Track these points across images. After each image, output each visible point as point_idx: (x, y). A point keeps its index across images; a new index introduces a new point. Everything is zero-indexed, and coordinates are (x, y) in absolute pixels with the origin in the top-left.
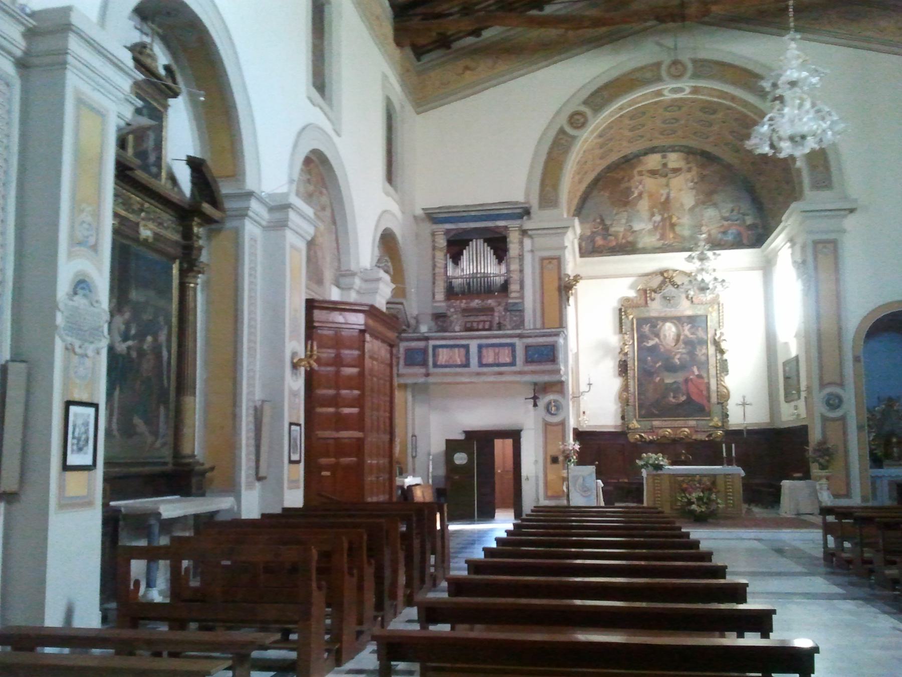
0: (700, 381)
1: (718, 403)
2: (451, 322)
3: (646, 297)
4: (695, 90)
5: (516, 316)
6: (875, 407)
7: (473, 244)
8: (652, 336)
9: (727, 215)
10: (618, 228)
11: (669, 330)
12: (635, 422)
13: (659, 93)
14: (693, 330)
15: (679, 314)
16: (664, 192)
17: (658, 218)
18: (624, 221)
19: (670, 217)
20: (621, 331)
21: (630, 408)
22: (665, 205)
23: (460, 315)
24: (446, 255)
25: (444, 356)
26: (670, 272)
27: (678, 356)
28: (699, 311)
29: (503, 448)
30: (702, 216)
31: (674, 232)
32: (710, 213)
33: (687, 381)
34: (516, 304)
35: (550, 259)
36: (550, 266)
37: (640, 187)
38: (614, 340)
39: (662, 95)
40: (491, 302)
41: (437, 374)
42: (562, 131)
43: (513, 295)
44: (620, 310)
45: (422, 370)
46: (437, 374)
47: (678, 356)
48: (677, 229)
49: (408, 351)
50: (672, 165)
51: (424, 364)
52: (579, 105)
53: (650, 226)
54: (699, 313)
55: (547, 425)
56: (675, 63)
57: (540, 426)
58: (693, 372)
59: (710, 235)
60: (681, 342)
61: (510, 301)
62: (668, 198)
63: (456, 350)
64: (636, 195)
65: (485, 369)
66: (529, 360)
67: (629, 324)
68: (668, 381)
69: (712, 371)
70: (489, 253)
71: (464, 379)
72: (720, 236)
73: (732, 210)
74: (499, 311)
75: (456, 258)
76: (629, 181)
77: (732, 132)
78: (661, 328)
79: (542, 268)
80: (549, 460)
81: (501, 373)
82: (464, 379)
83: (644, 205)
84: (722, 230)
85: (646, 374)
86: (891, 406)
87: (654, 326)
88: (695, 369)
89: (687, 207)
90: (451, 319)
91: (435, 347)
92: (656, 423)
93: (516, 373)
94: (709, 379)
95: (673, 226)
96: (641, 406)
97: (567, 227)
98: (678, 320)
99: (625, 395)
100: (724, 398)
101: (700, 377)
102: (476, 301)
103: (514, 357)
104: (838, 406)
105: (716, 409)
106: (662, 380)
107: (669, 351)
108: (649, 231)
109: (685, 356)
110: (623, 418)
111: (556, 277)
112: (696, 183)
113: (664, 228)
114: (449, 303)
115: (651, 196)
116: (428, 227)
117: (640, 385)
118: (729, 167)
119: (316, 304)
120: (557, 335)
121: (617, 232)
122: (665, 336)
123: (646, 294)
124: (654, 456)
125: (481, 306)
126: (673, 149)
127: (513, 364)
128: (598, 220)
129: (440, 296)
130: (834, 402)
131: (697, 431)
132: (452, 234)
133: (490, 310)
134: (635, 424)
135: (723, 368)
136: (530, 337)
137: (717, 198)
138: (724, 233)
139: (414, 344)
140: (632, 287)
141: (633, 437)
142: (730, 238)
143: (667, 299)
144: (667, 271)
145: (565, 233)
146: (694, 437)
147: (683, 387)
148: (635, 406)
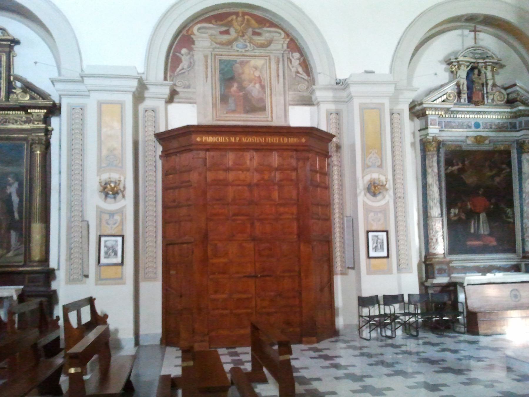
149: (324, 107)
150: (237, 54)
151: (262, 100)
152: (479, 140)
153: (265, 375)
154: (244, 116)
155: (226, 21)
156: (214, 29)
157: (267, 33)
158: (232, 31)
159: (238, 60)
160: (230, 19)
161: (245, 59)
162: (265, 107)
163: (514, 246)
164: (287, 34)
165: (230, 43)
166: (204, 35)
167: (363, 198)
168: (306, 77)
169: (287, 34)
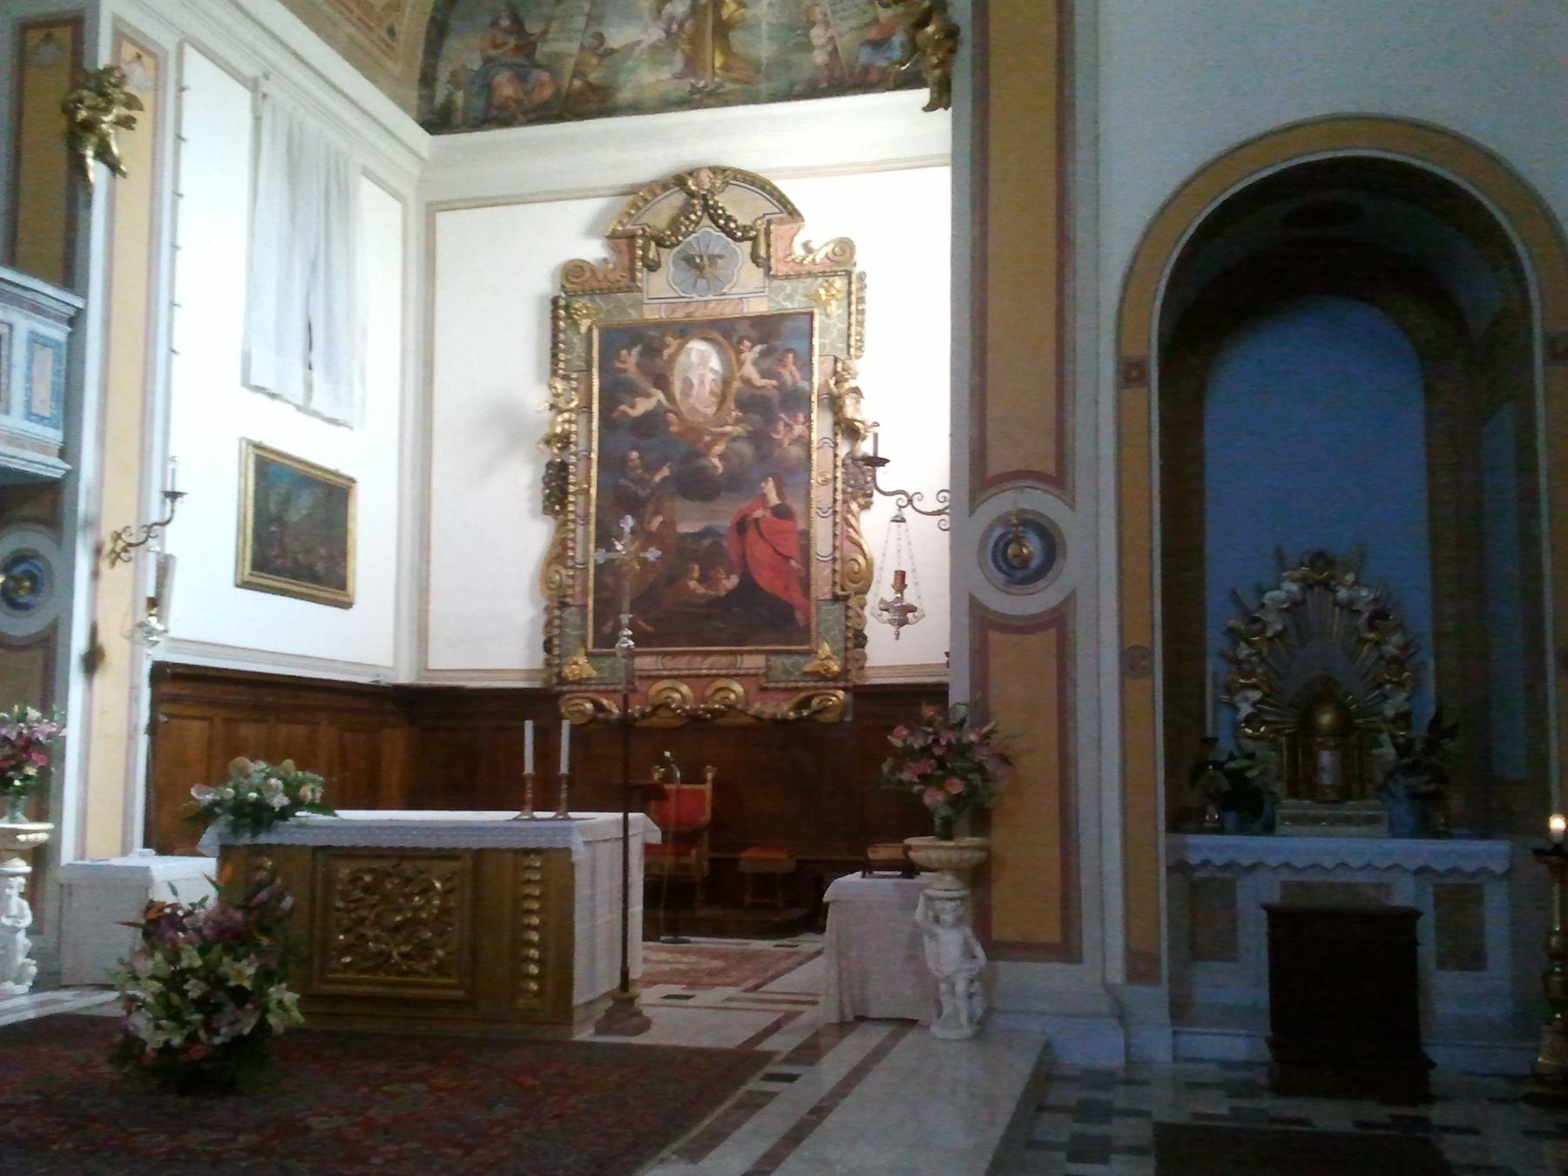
1: (836, 599)
3: (633, 259)
10: (564, 45)
11: (701, 363)
12: (582, 660)
14: (767, 363)
15: (729, 311)
18: (580, 22)
20: (554, 373)
21: (571, 615)
26: (705, 177)
27: (719, 448)
28: (790, 299)
31: (727, 51)
33: (742, 525)
35: (46, 25)
36: (48, 53)
44: (555, 301)
47: (719, 448)
48: (736, 38)
53: (656, 34)
54: (790, 306)
58: (764, 498)
69: (821, 495)
72: (865, 56)
78: (673, 358)
84: (872, 33)
87: (652, 351)
98: (724, 332)
101: (782, 512)
105: (826, 617)
107: (693, 432)
108: (655, 48)
110: (548, 646)
113: (696, 42)
121: (558, 56)
122: (688, 384)
123: (635, 244)
128: (505, 23)
131: (763, 689)
134: (580, 666)
138: (878, 45)
140: (592, 231)
143: (695, 265)
146: (757, 707)
148: (585, 606)
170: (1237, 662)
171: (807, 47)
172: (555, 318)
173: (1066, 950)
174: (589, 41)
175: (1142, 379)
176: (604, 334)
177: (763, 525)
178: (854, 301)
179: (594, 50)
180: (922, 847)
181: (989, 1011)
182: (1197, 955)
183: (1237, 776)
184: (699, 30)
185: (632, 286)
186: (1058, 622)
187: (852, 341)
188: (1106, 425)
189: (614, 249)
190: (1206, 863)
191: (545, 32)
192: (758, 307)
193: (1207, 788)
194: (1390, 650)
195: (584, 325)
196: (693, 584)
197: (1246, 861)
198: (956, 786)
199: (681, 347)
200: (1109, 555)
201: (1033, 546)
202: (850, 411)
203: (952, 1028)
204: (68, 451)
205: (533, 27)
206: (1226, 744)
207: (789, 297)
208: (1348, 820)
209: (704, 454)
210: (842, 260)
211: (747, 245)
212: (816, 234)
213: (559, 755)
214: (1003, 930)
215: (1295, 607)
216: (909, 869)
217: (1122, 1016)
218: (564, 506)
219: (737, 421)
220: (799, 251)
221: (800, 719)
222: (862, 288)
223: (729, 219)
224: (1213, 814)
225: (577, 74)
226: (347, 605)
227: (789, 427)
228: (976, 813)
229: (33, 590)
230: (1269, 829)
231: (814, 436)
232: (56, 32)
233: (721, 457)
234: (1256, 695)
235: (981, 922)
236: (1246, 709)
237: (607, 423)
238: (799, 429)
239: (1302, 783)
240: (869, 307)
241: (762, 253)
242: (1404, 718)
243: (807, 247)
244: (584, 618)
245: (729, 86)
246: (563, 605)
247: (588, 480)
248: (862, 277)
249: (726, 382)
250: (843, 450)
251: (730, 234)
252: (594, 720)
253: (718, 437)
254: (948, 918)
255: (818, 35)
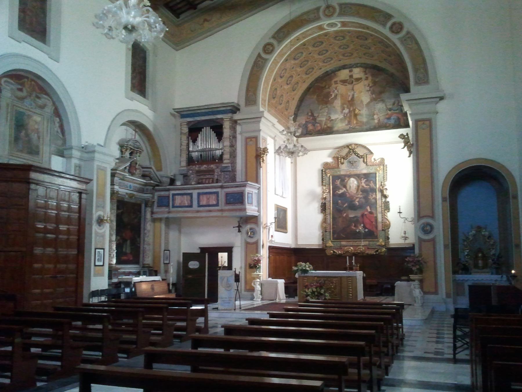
0: (371, 215)
1: (383, 230)
2: (190, 180)
3: (338, 162)
4: (344, 24)
5: (227, 175)
6: (468, 233)
7: (204, 130)
8: (341, 187)
9: (391, 107)
10: (322, 119)
11: (353, 183)
12: (330, 242)
13: (321, 28)
14: (367, 183)
15: (358, 172)
16: (350, 94)
17: (346, 111)
18: (325, 114)
19: (354, 110)
20: (322, 185)
21: (328, 233)
22: (351, 103)
23: (195, 175)
24: (188, 138)
25: (178, 200)
26: (353, 146)
27: (357, 200)
28: (371, 170)
29: (223, 257)
30: (375, 108)
31: (357, 120)
32: (380, 106)
33: (363, 215)
34: (226, 167)
35: (250, 138)
36: (251, 143)
37: (336, 91)
38: (319, 190)
39: (323, 29)
40: (213, 166)
41: (174, 212)
42: (259, 55)
43: (225, 161)
44: (322, 170)
45: (167, 210)
46: (174, 212)
47: (357, 200)
48: (359, 117)
49: (160, 197)
50: (355, 76)
51: (168, 206)
52: (270, 39)
53: (342, 116)
54: (371, 171)
55: (247, 244)
56: (328, 7)
57: (243, 244)
58: (367, 210)
59: (379, 120)
60: (360, 191)
61: (223, 165)
62: (353, 98)
63: (185, 196)
64: (333, 96)
65: (201, 209)
66: (228, 203)
67: (327, 179)
68: (351, 216)
69: (379, 209)
70: (213, 134)
71: (204, 214)
72: (386, 121)
73: (394, 104)
74: (217, 172)
75: (194, 141)
76: (329, 88)
77: (382, 51)
78: (347, 181)
79: (246, 144)
80: (248, 267)
81: (210, 211)
82: (204, 214)
83: (338, 103)
84: (387, 116)
85: (338, 211)
86: (480, 232)
87: (343, 180)
88: (368, 208)
89: (365, 103)
90: (190, 177)
91: (174, 195)
92: (344, 243)
93: (219, 211)
94: (377, 214)
95: (356, 115)
96: (334, 233)
97: (261, 117)
98: (358, 177)
99: (325, 225)
100: (386, 226)
101: (371, 213)
102: (205, 166)
103: (218, 200)
104: (430, 232)
105: (381, 234)
106: (347, 215)
107: (352, 197)
108: (341, 119)
109: (361, 199)
110: (323, 240)
111: (254, 149)
112: (370, 87)
113: (350, 117)
114: (189, 167)
115: (342, 96)
116: (180, 120)
117: (334, 218)
118: (392, 75)
119: (33, 168)
120: (245, 186)
121: (321, 121)
122: (350, 187)
123: (338, 159)
124: (304, 264)
125: (205, 169)
126: (356, 66)
127: (217, 205)
128: (310, 114)
129: (184, 164)
130: (427, 229)
131: (368, 248)
132: (191, 125)
133: (212, 172)
134: (330, 244)
135: (387, 207)
136: (228, 188)
137: (385, 96)
138: (389, 119)
139: (163, 193)
140: (329, 156)
141: (330, 252)
142: (392, 122)
143: (351, 163)
144: (350, 145)
145: (259, 122)
146: (367, 252)
147: (360, 220)
148: (330, 232)
149: (75, 161)
150: (26, 108)
151: (38, 147)
152: (131, 196)
153: (4, 351)
154: (27, 156)
155: (21, 82)
156: (14, 86)
157: (44, 100)
158: (24, 90)
159: (26, 114)
160: (23, 81)
161: (30, 113)
162: (39, 152)
163: (139, 260)
164: (54, 103)
165: (22, 99)
166: (8, 87)
167: (95, 227)
168: (61, 136)
169: (54, 103)
170: (464, 245)
171: (373, 119)
172: (322, 174)
173: (436, 293)
174: (327, 118)
175: (446, 201)
176: (332, 177)
177: (367, 216)
178: (385, 170)
179: (328, 120)
180: (412, 277)
181: (424, 303)
182: (458, 295)
183: (464, 265)
184: (350, 116)
185: (338, 167)
186: (433, 241)
187: (384, 178)
188: (441, 209)
189: (335, 160)
190: (459, 280)
191: (318, 116)
192: (365, 171)
193: (459, 267)
194: (491, 243)
195: (328, 175)
196: (353, 227)
197: (466, 279)
198: (418, 267)
199: (349, 179)
200: (441, 230)
201: (428, 228)
202: (385, 193)
203: (417, 305)
204: (259, 211)
205: (316, 115)
206: (463, 259)
207: (371, 170)
208: (484, 272)
209: (354, 201)
210: (382, 162)
211: (362, 159)
212: (376, 156)
213: (91, 253)
214: (426, 289)
215: (474, 235)
216: (409, 280)
217: (445, 303)
218: (325, 211)
219: (361, 194)
220: (373, 160)
221: (376, 254)
222: (386, 168)
223: (358, 154)
224: (460, 272)
225: (325, 124)
226: (286, 233)
227: (372, 196)
228: (421, 271)
229: (254, 234)
230: (470, 274)
231: (377, 198)
232: (253, 139)
233: (358, 202)
234: (468, 251)
235: (422, 288)
236: (466, 253)
237: (334, 195)
238: (374, 196)
239: (476, 266)
240: (388, 171)
241: (365, 161)
242: (494, 255)
243: (374, 159)
244: (330, 234)
245: (357, 127)
246: (326, 231)
247: (330, 206)
248: (386, 165)
249: (358, 186)
250: (384, 200)
251: (358, 157)
252: (333, 254)
253: (357, 198)
254: (417, 287)
255: (376, 117)
